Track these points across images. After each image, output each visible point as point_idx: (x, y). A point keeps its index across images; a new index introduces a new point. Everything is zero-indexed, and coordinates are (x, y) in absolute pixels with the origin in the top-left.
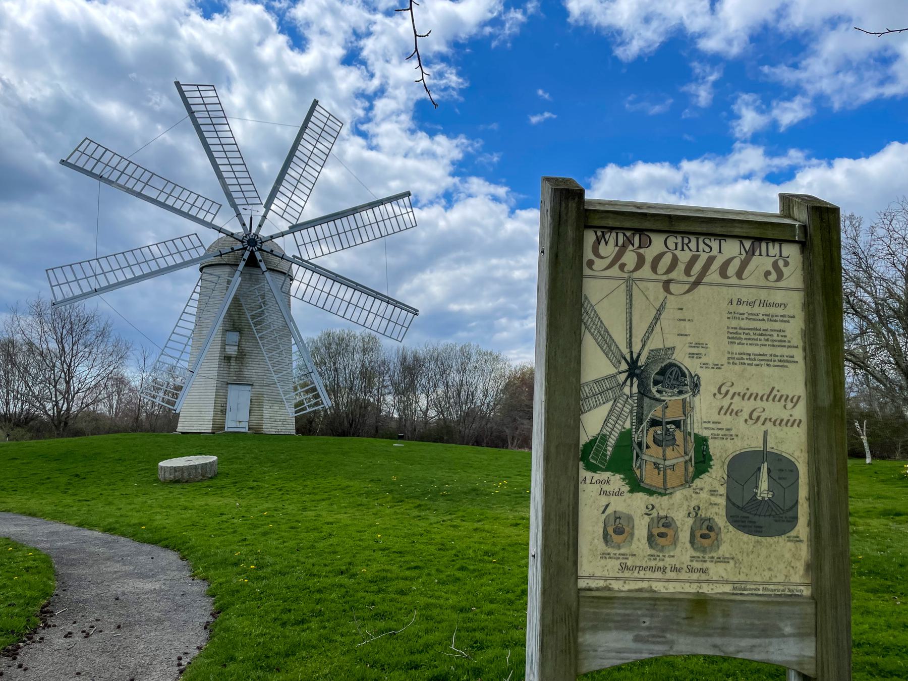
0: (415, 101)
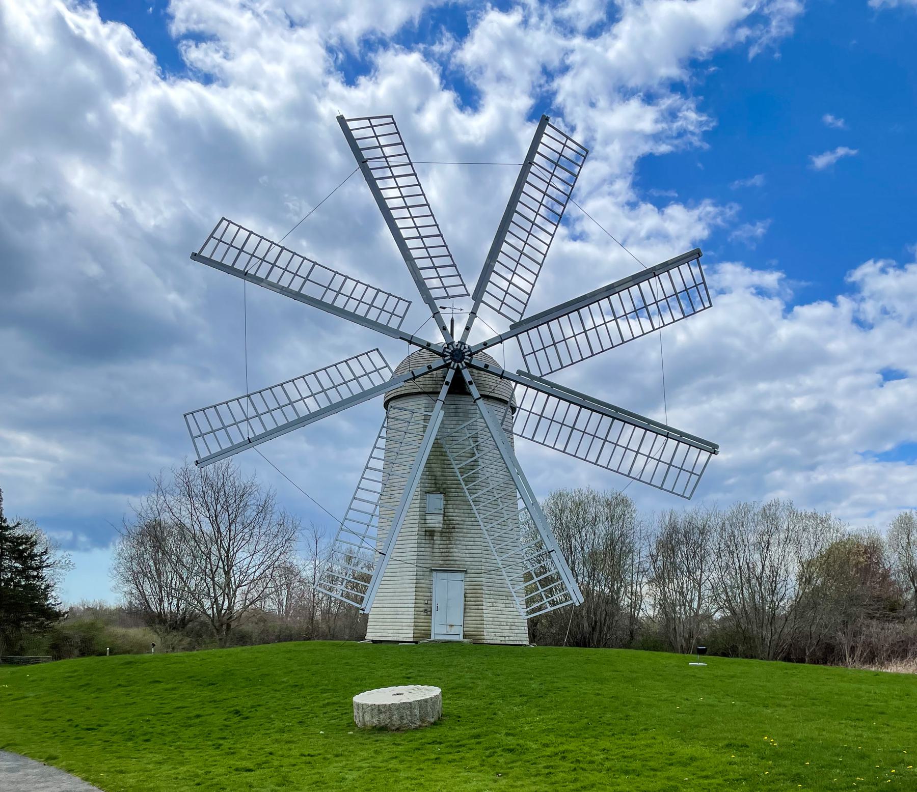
0: (635, 159)
